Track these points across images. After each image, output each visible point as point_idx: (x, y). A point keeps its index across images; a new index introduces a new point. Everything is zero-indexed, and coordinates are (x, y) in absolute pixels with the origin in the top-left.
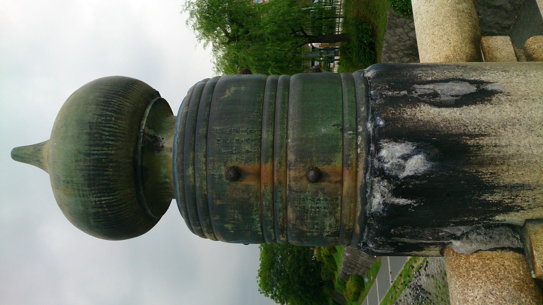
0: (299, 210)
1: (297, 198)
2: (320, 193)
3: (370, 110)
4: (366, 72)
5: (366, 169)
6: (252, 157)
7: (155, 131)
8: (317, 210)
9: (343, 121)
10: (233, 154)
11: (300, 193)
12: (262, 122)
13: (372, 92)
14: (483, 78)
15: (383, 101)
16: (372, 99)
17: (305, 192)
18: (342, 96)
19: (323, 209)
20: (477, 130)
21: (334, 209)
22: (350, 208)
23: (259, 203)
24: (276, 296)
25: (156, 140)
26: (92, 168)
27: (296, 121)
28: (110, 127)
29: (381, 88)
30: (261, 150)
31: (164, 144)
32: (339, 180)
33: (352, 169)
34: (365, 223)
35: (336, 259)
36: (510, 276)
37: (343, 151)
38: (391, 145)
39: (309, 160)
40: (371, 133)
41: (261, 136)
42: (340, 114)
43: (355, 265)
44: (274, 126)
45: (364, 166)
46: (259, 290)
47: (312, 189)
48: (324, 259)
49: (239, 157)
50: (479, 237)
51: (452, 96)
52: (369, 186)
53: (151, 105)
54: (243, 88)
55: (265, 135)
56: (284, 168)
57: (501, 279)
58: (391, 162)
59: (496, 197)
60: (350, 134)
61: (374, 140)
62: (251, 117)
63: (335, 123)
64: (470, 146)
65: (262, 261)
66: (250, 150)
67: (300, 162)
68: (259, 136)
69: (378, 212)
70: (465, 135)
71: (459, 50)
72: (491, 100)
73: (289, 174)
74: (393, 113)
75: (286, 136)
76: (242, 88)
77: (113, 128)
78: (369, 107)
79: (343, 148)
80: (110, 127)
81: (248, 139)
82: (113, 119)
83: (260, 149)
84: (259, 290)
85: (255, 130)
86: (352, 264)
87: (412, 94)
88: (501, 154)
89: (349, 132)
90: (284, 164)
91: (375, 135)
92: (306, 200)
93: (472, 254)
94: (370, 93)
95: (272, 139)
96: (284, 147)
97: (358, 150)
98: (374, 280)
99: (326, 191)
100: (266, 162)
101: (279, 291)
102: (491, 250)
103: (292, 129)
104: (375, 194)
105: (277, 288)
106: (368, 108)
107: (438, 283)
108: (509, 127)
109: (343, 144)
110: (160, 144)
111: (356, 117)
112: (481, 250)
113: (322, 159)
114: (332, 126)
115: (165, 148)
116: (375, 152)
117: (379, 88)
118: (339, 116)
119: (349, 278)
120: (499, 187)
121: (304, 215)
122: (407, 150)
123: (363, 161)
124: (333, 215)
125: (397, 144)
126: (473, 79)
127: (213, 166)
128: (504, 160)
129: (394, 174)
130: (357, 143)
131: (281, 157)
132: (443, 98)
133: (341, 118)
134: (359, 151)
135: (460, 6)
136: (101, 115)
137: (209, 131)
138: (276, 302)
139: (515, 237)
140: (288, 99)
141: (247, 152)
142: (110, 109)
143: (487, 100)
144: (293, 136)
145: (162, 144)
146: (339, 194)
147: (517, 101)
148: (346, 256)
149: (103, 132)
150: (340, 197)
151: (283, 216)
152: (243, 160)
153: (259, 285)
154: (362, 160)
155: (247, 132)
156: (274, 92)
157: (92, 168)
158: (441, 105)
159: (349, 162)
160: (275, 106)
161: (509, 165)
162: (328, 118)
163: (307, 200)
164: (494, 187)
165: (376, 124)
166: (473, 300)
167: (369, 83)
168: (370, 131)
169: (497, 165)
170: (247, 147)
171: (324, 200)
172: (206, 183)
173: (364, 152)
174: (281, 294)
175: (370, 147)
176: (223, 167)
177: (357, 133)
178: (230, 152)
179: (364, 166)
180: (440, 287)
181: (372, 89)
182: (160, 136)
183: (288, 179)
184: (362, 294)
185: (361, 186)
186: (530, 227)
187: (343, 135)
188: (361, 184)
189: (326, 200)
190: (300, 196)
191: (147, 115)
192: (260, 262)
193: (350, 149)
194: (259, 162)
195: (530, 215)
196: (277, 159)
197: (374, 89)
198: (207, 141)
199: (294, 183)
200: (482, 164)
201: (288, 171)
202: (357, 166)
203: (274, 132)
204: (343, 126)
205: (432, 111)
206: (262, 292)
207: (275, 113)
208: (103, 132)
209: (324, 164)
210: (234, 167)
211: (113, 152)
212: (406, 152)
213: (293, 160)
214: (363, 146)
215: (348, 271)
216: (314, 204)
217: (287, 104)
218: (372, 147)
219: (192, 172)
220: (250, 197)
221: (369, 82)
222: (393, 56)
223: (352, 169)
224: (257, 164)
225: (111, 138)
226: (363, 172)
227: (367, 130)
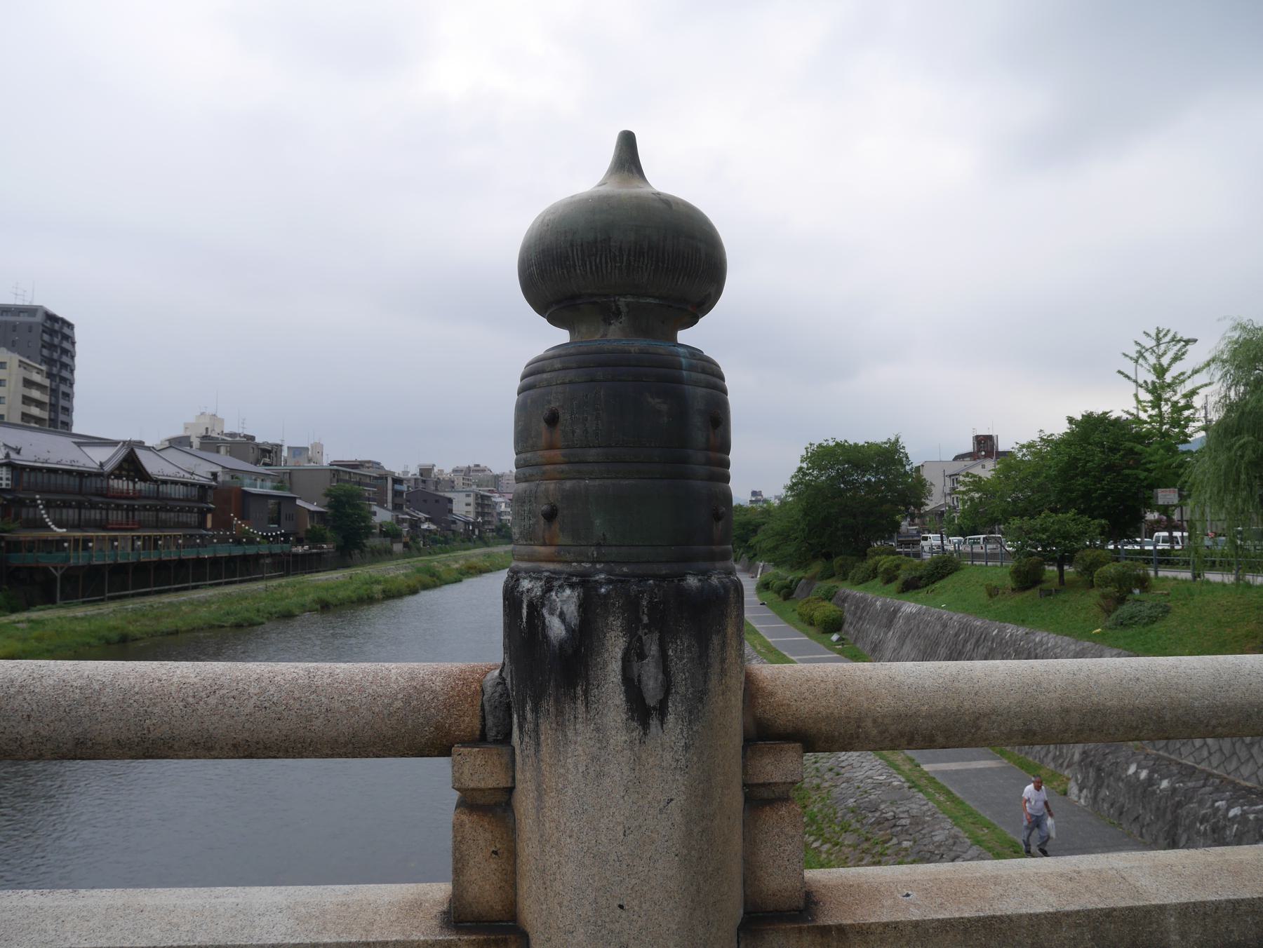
5: (554, 572)
13: (651, 582)
14: (671, 718)
15: (633, 593)
20: (593, 699)
23: (529, 449)
24: (803, 476)
26: (559, 250)
28: (606, 263)
35: (871, 583)
36: (453, 720)
38: (575, 600)
40: (593, 579)
43: (860, 618)
46: (811, 444)
48: (871, 562)
50: (497, 695)
51: (639, 676)
55: (593, 451)
57: (449, 711)
58: (558, 600)
59: (529, 716)
60: (593, 555)
61: (584, 581)
64: (575, 689)
65: (863, 446)
70: (588, 684)
71: (782, 710)
72: (633, 720)
74: (614, 604)
77: (607, 267)
80: (606, 263)
82: (618, 265)
84: (811, 444)
86: (862, 613)
87: (644, 629)
88: (567, 723)
89: (595, 553)
93: (481, 686)
98: (834, 650)
101: (812, 480)
102: (482, 705)
105: (817, 478)
106: (625, 575)
107: (822, 760)
108: (597, 735)
112: (484, 695)
119: (838, 606)
120: (537, 718)
122: (570, 618)
125: (577, 607)
126: (670, 704)
128: (561, 726)
129: (546, 602)
132: (635, 666)
135: (869, 723)
136: (620, 249)
138: (793, 477)
139: (498, 733)
141: (573, 432)
142: (632, 258)
143: (632, 715)
147: (632, 750)
148: (876, 601)
149: (598, 256)
153: (820, 444)
157: (559, 250)
158: (626, 660)
161: (556, 730)
164: (537, 713)
166: (431, 680)
169: (556, 717)
174: (808, 485)
175: (577, 576)
180: (816, 762)
182: (623, 318)
184: (812, 630)
186: (504, 749)
191: (642, 301)
192: (861, 443)
195: (518, 752)
200: (557, 701)
202: (559, 562)
205: (617, 649)
206: (809, 450)
208: (598, 256)
211: (578, 271)
212: (567, 617)
215: (851, 606)
225: (594, 268)
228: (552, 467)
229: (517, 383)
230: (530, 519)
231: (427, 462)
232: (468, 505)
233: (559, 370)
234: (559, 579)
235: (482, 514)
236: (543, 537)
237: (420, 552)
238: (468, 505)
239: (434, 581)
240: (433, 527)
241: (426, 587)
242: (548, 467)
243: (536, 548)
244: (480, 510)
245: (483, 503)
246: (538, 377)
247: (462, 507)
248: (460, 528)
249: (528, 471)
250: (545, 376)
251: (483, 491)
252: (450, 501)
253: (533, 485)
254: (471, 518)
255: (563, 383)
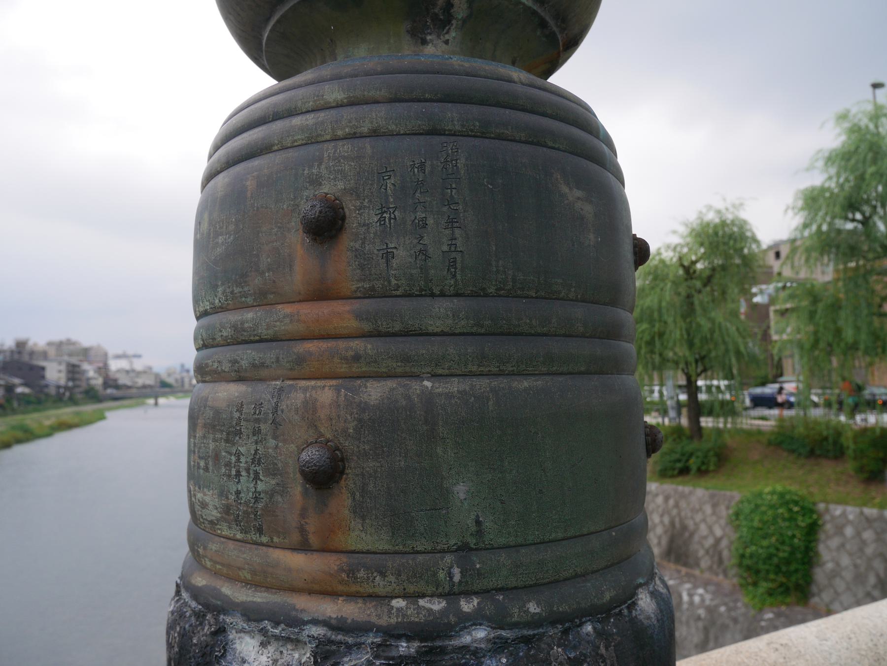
0: (232, 418)
1: (260, 413)
2: (273, 482)
3: (531, 632)
4: (651, 588)
5: (340, 626)
6: (373, 271)
7: (464, 21)
8: (234, 472)
9: (493, 548)
10: (383, 213)
11: (274, 421)
12: (486, 295)
13: (589, 628)
16: (566, 632)
17: (275, 437)
18: (576, 537)
19: (235, 489)
21: (237, 521)
22: (239, 569)
23: (250, 300)
25: (443, 22)
27: (491, 403)
29: (602, 656)
30: (397, 296)
31: (430, 45)
32: (311, 541)
33: (341, 582)
34: (209, 607)
37: (396, 553)
39: (367, 447)
40: (456, 642)
41: (439, 296)
42: (517, 536)
44: (472, 334)
45: (349, 621)
47: (227, 471)
49: (372, 230)
52: (291, 632)
53: (535, 8)
54: (591, 238)
55: (442, 306)
56: (343, 370)
60: (450, 576)
61: (431, 651)
62: (501, 262)
63: (488, 524)
66: (395, 263)
67: (360, 420)
68: (439, 288)
69: (225, 650)
73: (324, 387)
75: (440, 371)
76: (592, 236)
78: (541, 626)
79: (405, 553)
81: (427, 257)
83: (398, 293)
85: (459, 277)
90: (354, 369)
91: (447, 654)
92: (255, 438)
94: (586, 622)
95: (431, 329)
96: (408, 369)
97: (400, 600)
99: (280, 499)
100: (359, 316)
103: (465, 391)
104: (271, 649)
106: (536, 622)
109: (418, 552)
110: (430, 34)
111: (507, 589)
113: (371, 487)
114: (477, 516)
115: (421, 48)
116: (393, 658)
117: (602, 650)
118: (509, 533)
121: (222, 431)
123: (367, 619)
124: (224, 515)
127: (344, 158)
130: (423, 596)
131: (375, 362)
133: (502, 541)
134: (399, 603)
137: (453, 138)
140: (561, 374)
141: (388, 256)
144: (440, 395)
145: (431, 41)
146: (272, 539)
150: (265, 539)
151: (222, 370)
152: (363, 243)
154: (369, 615)
155: (450, 251)
156: (581, 329)
159: (362, 574)
160: (539, 335)
162: (502, 502)
163: (256, 443)
165: (484, 656)
167: (617, 610)
168: (459, 636)
170: (402, 255)
171: (255, 491)
172: (299, 143)
173: (393, 621)
175: (409, 639)
176: (341, 185)
177: (454, 594)
178: (387, 201)
179: (349, 621)
181: (599, 626)
182: (453, 34)
183: (313, 383)
185: (294, 608)
187: (448, 551)
188: (297, 607)
189: (257, 499)
190: (265, 422)
193: (404, 577)
194: (359, 295)
196: (369, 346)
197: (599, 633)
198: (421, 134)
199: (299, 403)
201: (334, 382)
202: (352, 596)
203: (454, 334)
204: (476, 549)
207: (516, 334)
209: (353, 494)
210: (343, 218)
213: (365, 397)
214: (414, 617)
216: (246, 462)
217: (544, 369)
218: (408, 647)
219: (331, 100)
220: (262, 273)
221: (620, 611)
222: (671, 502)
223: (341, 582)
224: (354, 287)
226: (330, 617)
227: (465, 628)
228: (324, 345)
229: (201, 165)
230: (257, 478)
231: (22, 335)
232: (60, 371)
233: (339, 105)
234: (359, 645)
235: (73, 379)
236: (302, 530)
237: (14, 412)
238: (60, 371)
239: (27, 436)
240: (26, 390)
241: (19, 441)
242: (311, 346)
243: (277, 554)
244: (70, 375)
245: (74, 371)
246: (278, 126)
247: (55, 374)
248: (52, 391)
249: (222, 357)
250: (297, 121)
251: (74, 360)
252: (43, 369)
253: (264, 392)
254: (63, 382)
255: (353, 136)
